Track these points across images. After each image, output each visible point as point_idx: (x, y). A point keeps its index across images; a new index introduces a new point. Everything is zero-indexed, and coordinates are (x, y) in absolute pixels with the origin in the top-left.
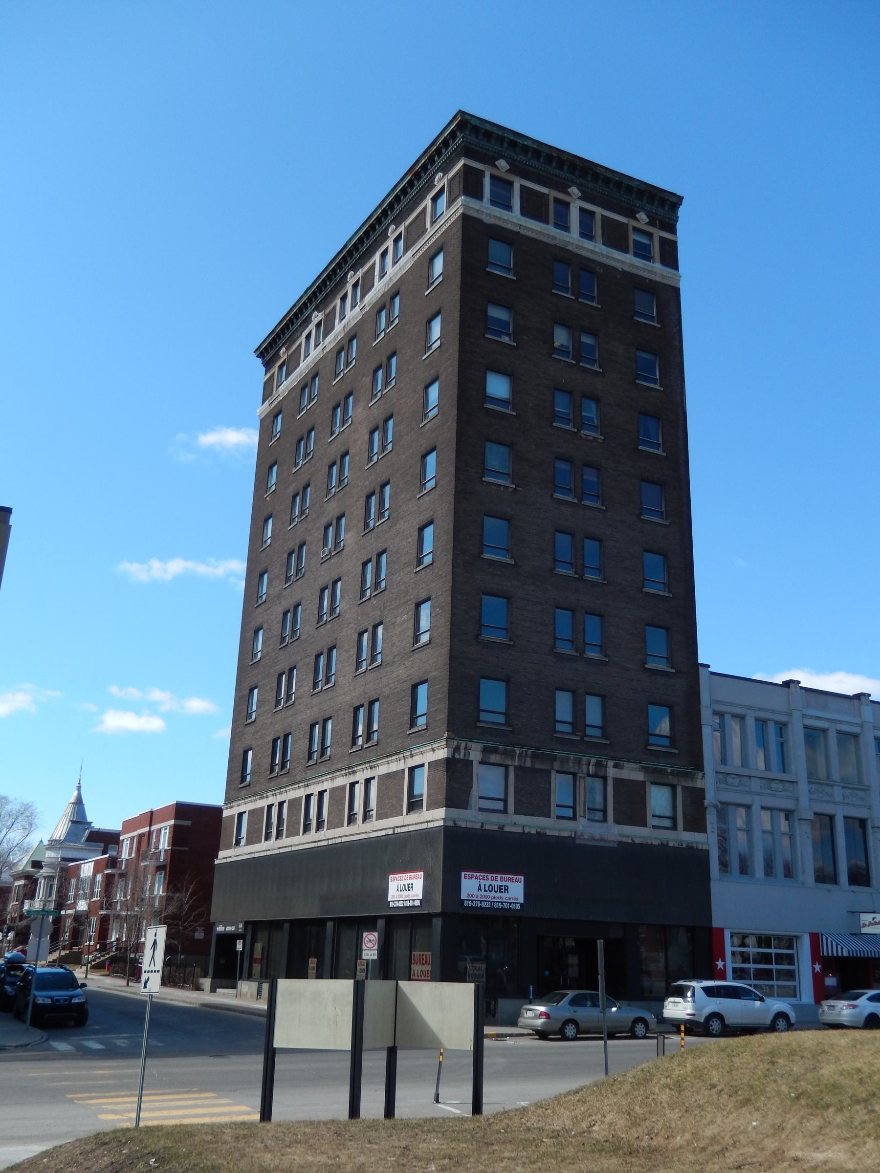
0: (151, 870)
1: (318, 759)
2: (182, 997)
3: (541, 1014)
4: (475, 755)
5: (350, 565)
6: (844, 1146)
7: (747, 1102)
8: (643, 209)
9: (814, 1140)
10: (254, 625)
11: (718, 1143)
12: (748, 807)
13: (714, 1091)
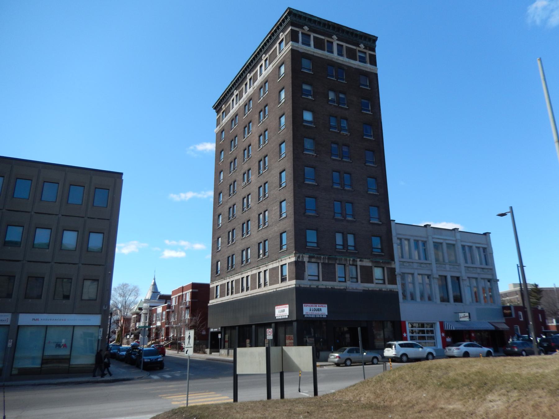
0: (184, 309)
1: (245, 263)
2: (208, 355)
3: (337, 357)
4: (306, 259)
5: (253, 188)
6: (460, 402)
7: (420, 387)
8: (362, 43)
9: (448, 401)
10: (217, 213)
11: (411, 403)
12: (413, 274)
13: (407, 383)
